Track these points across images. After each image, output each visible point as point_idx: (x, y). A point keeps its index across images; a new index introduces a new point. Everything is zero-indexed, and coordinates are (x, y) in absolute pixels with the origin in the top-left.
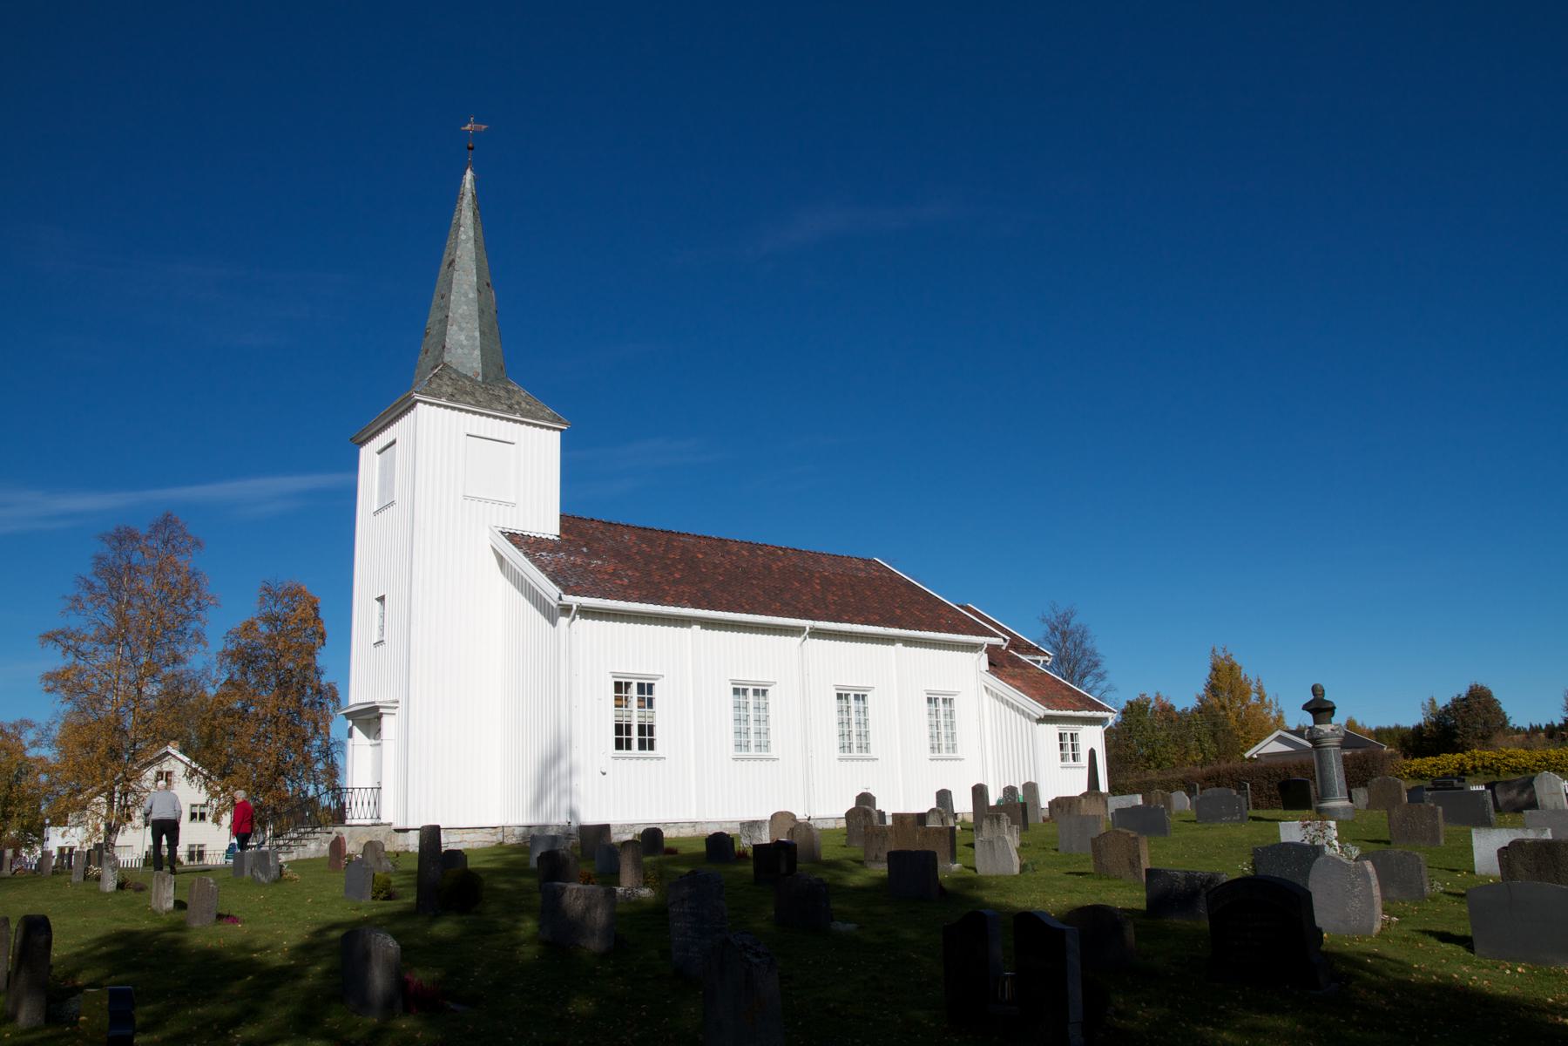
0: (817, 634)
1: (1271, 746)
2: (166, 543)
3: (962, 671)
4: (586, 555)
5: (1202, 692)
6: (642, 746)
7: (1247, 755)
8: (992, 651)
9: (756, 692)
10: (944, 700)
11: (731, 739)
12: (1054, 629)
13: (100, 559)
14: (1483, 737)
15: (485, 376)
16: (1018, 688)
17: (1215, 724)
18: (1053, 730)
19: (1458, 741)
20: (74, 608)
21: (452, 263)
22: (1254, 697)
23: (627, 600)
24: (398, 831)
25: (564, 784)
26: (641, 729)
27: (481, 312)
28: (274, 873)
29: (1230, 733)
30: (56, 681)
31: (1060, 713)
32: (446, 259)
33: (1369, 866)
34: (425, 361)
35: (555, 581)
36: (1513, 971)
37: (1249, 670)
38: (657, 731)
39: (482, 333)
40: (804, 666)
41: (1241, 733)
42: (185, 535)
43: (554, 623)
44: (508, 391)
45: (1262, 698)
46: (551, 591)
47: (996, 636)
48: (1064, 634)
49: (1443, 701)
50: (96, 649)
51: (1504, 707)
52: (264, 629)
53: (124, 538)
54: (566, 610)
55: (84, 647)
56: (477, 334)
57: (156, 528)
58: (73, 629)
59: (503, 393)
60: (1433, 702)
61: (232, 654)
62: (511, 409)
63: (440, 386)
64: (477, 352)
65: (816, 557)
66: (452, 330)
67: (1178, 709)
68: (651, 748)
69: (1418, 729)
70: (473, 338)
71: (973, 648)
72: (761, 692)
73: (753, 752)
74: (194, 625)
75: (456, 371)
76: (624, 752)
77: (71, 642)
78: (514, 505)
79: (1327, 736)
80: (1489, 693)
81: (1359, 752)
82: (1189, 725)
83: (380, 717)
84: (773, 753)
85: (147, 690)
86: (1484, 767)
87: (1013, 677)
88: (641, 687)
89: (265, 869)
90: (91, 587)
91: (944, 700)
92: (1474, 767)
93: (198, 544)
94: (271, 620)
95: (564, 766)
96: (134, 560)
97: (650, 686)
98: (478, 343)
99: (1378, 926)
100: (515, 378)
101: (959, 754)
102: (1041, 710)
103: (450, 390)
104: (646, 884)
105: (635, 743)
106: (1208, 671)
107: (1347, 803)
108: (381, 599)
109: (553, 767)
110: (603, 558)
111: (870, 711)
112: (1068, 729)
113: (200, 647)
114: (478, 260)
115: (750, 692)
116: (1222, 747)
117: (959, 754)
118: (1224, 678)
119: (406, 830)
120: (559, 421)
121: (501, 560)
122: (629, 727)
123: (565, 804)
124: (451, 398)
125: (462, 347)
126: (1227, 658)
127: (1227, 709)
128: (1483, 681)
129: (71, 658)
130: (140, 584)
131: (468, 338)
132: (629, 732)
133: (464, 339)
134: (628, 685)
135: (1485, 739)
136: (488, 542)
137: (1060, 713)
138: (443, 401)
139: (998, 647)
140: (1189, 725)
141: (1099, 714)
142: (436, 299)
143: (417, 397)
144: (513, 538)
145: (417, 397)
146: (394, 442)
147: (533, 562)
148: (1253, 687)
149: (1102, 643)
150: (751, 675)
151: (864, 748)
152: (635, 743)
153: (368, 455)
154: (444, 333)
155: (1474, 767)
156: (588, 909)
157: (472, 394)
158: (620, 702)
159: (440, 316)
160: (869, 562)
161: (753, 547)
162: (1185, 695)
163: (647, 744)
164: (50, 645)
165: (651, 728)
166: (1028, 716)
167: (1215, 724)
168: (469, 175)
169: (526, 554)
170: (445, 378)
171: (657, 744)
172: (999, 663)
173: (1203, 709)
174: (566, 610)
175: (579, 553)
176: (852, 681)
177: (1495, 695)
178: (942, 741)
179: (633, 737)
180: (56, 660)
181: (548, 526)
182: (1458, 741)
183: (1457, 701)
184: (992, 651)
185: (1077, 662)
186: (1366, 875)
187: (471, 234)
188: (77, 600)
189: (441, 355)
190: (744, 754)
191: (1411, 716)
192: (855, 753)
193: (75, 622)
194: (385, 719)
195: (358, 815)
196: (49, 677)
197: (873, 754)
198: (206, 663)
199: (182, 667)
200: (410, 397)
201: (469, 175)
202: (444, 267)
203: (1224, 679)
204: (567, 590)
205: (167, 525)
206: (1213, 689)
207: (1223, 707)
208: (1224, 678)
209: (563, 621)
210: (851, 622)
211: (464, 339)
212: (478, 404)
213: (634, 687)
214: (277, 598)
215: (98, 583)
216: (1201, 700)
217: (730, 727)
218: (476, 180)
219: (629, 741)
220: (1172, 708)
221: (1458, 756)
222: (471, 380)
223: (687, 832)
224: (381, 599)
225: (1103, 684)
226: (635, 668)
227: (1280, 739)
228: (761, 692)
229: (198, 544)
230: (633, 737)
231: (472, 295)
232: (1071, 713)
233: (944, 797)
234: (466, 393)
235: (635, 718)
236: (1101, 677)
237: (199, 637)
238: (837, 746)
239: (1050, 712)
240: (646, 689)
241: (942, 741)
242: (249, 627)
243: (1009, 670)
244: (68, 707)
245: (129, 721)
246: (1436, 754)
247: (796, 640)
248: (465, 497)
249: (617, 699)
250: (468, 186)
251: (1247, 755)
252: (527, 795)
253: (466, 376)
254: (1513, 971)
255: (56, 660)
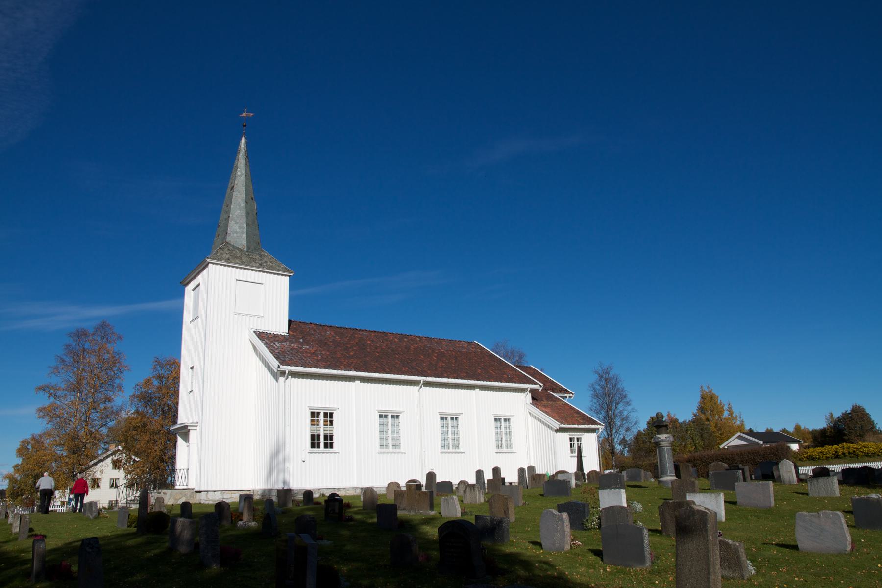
0: (427, 384)
1: (734, 441)
2: (102, 337)
3: (516, 404)
4: (302, 343)
5: (695, 411)
6: (326, 446)
7: (721, 447)
8: (533, 391)
9: (393, 417)
10: (505, 420)
11: (378, 442)
12: (601, 377)
13: (68, 346)
14: (860, 435)
15: (248, 248)
16: (546, 413)
17: (702, 429)
18: (566, 436)
19: (846, 437)
20: (54, 373)
21: (232, 188)
22: (726, 414)
23: (317, 367)
24: (197, 492)
25: (281, 466)
26: (326, 437)
27: (248, 214)
28: (95, 514)
29: (711, 435)
30: (44, 412)
31: (569, 426)
32: (230, 186)
33: (565, 515)
34: (218, 240)
35: (277, 358)
36: (605, 570)
37: (723, 398)
38: (334, 438)
39: (248, 225)
40: (421, 403)
41: (718, 434)
42: (113, 333)
43: (277, 380)
44: (261, 256)
45: (731, 414)
46: (274, 363)
47: (536, 383)
48: (606, 380)
49: (837, 415)
50: (65, 395)
51: (874, 418)
52: (156, 383)
53: (81, 334)
54: (283, 373)
55: (59, 393)
56: (245, 225)
57: (97, 329)
58: (53, 384)
59: (258, 257)
60: (831, 415)
61: (138, 397)
62: (261, 265)
63: (222, 254)
64: (245, 235)
65: (439, 341)
66: (231, 224)
67: (681, 421)
68: (332, 447)
69: (823, 432)
70: (243, 228)
71: (523, 390)
72: (395, 417)
73: (390, 449)
74: (117, 381)
75: (233, 246)
76: (316, 450)
77: (52, 391)
78: (262, 317)
79: (662, 441)
80: (863, 409)
81: (774, 445)
82: (687, 430)
83: (189, 431)
84: (402, 450)
85: (93, 416)
86: (849, 453)
87: (545, 406)
88: (326, 414)
89: (91, 512)
90: (63, 361)
91: (505, 420)
92: (843, 453)
93: (120, 338)
94: (160, 378)
95: (281, 457)
96: (86, 347)
97: (331, 414)
98: (245, 230)
99: (567, 547)
100: (257, 254)
101: (513, 450)
102: (557, 425)
103: (227, 256)
104: (254, 520)
105: (322, 445)
106: (699, 399)
107: (674, 478)
108: (192, 368)
109: (277, 458)
110: (308, 346)
111: (460, 426)
112: (575, 435)
113: (120, 393)
114: (247, 186)
115: (389, 417)
116: (706, 442)
117: (513, 450)
118: (708, 404)
119: (200, 492)
120: (288, 271)
121: (255, 348)
122: (319, 436)
123: (281, 477)
124: (228, 260)
125: (237, 233)
126: (710, 392)
127: (709, 422)
128: (859, 403)
129: (52, 399)
130: (89, 360)
131: (240, 228)
132: (318, 438)
133: (237, 230)
134: (318, 413)
135: (861, 437)
136: (248, 337)
137: (569, 426)
138: (223, 262)
139: (537, 390)
140: (687, 430)
141: (593, 427)
142: (224, 207)
143: (209, 260)
144: (261, 335)
145: (209, 260)
146: (199, 285)
147: (268, 348)
148: (725, 408)
149: (629, 385)
150: (390, 407)
151: (456, 446)
152: (322, 445)
153: (188, 289)
154: (227, 226)
155: (843, 453)
156: (181, 532)
157: (240, 258)
158: (313, 423)
159: (226, 216)
160: (470, 343)
161: (402, 336)
162: (685, 412)
163: (329, 445)
164: (41, 393)
165: (332, 437)
166: (551, 429)
167: (702, 429)
168: (243, 140)
169: (265, 344)
170: (226, 250)
171: (334, 445)
172: (536, 398)
173: (696, 422)
174: (283, 373)
175: (297, 342)
176: (449, 410)
177: (868, 411)
178: (503, 443)
179: (322, 441)
180: (45, 401)
181: (282, 329)
182: (846, 437)
183: (845, 415)
184: (533, 391)
185: (614, 396)
186: (562, 520)
187: (243, 172)
188: (57, 368)
189: (225, 238)
190: (384, 450)
191: (818, 423)
192: (505, 449)
193: (54, 380)
194: (191, 433)
195: (180, 484)
196: (40, 410)
197: (461, 450)
198: (124, 403)
199: (109, 405)
200: (205, 260)
201: (243, 140)
202: (229, 190)
203: (708, 404)
204: (283, 362)
205: (103, 328)
206: (702, 409)
207: (708, 420)
208: (708, 404)
209: (282, 379)
210: (448, 377)
211: (237, 230)
212: (243, 263)
213: (322, 415)
214: (162, 366)
215: (67, 359)
216: (695, 416)
217: (377, 435)
218: (247, 142)
219: (319, 444)
220: (677, 420)
221: (835, 447)
222: (240, 250)
223: (351, 493)
224: (192, 368)
225: (629, 408)
226: (323, 404)
227: (740, 437)
228: (395, 417)
229: (120, 338)
230: (322, 441)
231: (243, 205)
232: (576, 426)
233: (479, 474)
234: (237, 258)
235: (322, 430)
236: (628, 403)
237: (120, 388)
238: (495, 445)
239: (563, 426)
240: (329, 416)
241: (503, 443)
242: (148, 382)
243: (545, 402)
244: (50, 426)
245: (82, 433)
246: (822, 446)
247: (416, 388)
248: (235, 313)
249: (312, 421)
250: (242, 146)
251: (721, 447)
252: (264, 473)
253: (238, 249)
254: (605, 570)
255: (45, 401)
